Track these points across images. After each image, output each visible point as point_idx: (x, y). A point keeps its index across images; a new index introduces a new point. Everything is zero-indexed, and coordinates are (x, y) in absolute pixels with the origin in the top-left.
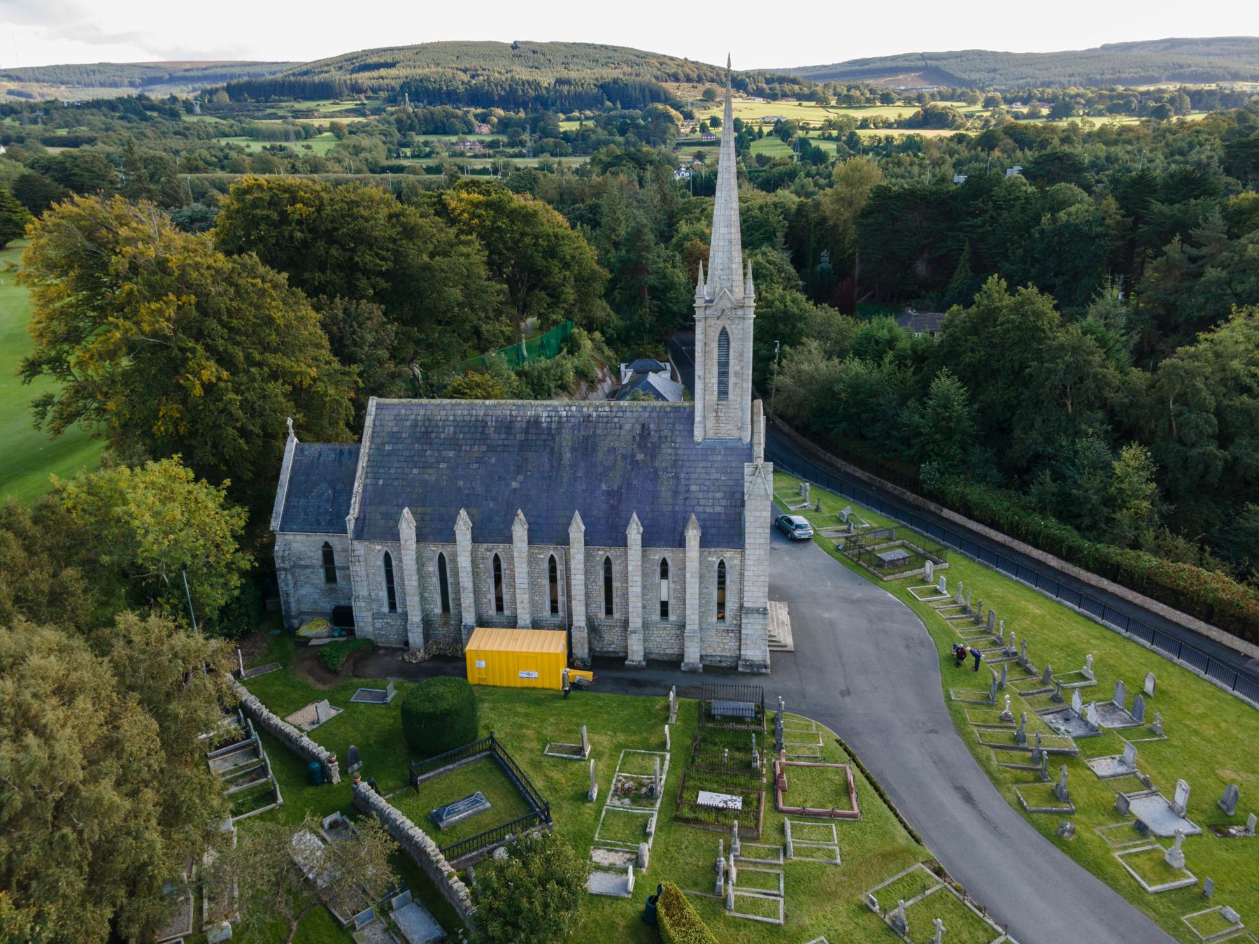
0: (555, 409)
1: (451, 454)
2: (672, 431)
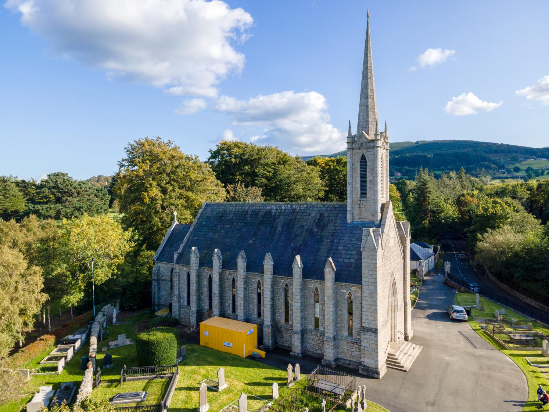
0: (280, 206)
1: (228, 226)
2: (336, 217)
